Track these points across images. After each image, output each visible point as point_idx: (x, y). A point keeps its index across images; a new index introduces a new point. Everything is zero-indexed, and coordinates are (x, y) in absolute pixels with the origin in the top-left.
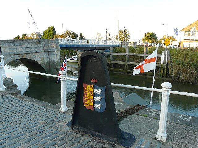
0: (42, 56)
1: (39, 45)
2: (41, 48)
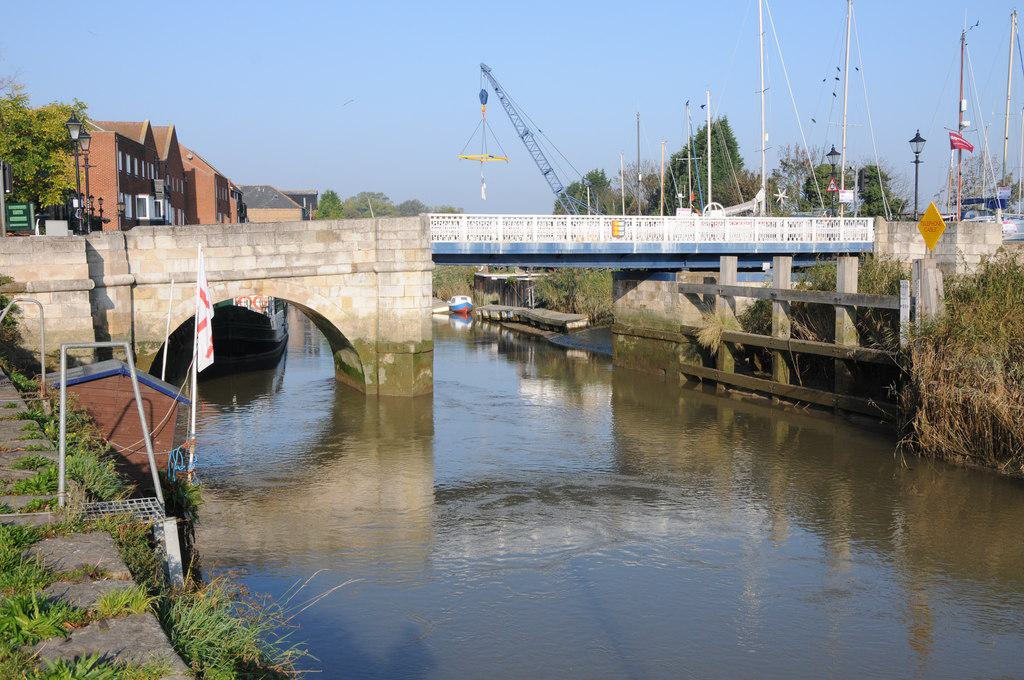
0: (345, 292)
1: (335, 246)
2: (341, 258)
